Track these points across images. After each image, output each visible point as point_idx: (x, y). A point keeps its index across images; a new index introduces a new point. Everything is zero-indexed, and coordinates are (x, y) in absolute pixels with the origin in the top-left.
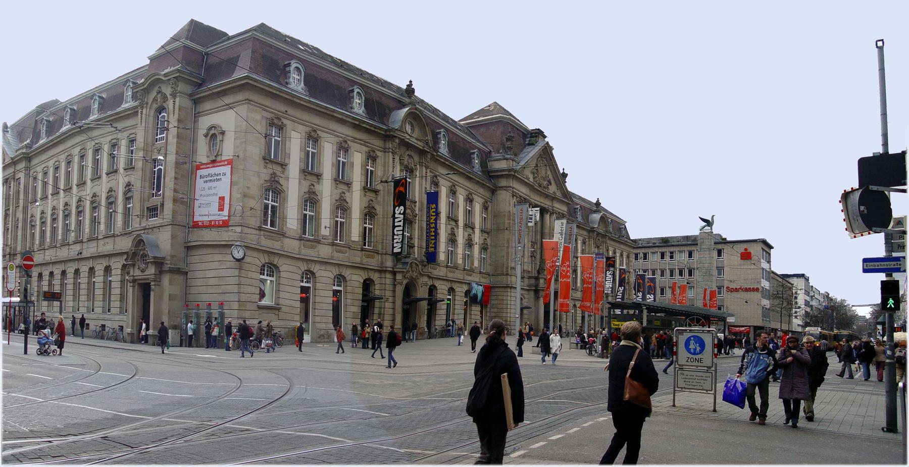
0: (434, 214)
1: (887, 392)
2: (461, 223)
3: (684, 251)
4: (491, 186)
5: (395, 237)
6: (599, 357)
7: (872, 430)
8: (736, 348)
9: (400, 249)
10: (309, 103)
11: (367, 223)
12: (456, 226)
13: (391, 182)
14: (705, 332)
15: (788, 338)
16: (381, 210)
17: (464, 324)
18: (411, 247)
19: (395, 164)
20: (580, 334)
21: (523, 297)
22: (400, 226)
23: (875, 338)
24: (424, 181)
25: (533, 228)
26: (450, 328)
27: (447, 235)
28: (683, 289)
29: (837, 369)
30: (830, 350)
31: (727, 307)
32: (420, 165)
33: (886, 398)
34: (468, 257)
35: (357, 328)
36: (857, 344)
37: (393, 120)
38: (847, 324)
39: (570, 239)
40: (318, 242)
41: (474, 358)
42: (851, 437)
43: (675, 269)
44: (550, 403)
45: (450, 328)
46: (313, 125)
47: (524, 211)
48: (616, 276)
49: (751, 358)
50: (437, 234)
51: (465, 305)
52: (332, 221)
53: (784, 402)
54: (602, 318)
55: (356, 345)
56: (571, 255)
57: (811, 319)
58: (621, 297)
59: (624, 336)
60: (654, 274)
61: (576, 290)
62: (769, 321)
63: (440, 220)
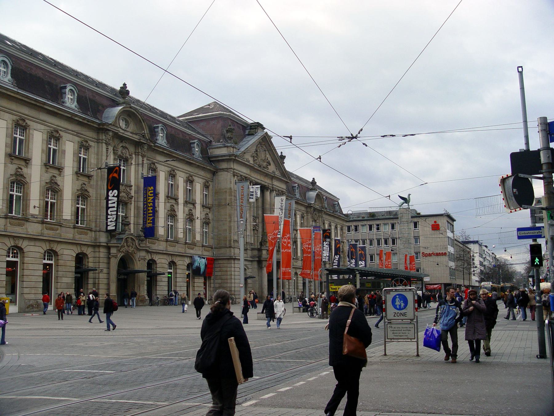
0: (152, 195)
1: (538, 328)
2: (181, 200)
3: (388, 223)
4: (212, 169)
5: (109, 217)
6: (320, 318)
7: (530, 358)
8: (432, 302)
9: (114, 227)
10: (17, 94)
11: (80, 204)
12: (176, 203)
13: (104, 168)
14: (407, 290)
15: (469, 292)
16: (94, 192)
17: (187, 295)
18: (126, 224)
19: (109, 153)
20: (302, 299)
21: (247, 267)
22: (114, 207)
23: (529, 288)
24: (140, 168)
25: (254, 204)
26: (173, 297)
27: (166, 211)
28: (388, 255)
29: (505, 313)
30: (499, 299)
31: (423, 269)
32: (135, 155)
33: (538, 333)
34: (189, 232)
35: (71, 297)
36: (517, 293)
37: (107, 116)
38: (509, 278)
39: (289, 214)
40: (27, 220)
41: (199, 324)
42: (517, 365)
43: (381, 239)
44: (277, 362)
45: (173, 297)
46: (21, 115)
47: (246, 188)
48: (332, 246)
49: (443, 309)
50: (155, 212)
51: (187, 278)
52: (42, 202)
53: (469, 343)
54: (321, 283)
55: (72, 313)
56: (291, 228)
57: (485, 276)
58: (337, 264)
59: (341, 298)
60: (364, 243)
61: (297, 259)
62: (455, 279)
63: (159, 200)
